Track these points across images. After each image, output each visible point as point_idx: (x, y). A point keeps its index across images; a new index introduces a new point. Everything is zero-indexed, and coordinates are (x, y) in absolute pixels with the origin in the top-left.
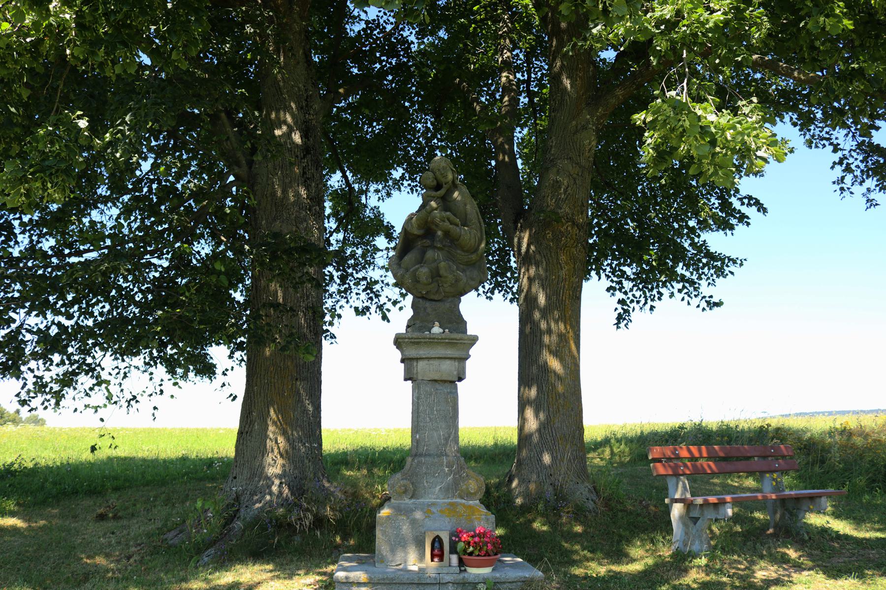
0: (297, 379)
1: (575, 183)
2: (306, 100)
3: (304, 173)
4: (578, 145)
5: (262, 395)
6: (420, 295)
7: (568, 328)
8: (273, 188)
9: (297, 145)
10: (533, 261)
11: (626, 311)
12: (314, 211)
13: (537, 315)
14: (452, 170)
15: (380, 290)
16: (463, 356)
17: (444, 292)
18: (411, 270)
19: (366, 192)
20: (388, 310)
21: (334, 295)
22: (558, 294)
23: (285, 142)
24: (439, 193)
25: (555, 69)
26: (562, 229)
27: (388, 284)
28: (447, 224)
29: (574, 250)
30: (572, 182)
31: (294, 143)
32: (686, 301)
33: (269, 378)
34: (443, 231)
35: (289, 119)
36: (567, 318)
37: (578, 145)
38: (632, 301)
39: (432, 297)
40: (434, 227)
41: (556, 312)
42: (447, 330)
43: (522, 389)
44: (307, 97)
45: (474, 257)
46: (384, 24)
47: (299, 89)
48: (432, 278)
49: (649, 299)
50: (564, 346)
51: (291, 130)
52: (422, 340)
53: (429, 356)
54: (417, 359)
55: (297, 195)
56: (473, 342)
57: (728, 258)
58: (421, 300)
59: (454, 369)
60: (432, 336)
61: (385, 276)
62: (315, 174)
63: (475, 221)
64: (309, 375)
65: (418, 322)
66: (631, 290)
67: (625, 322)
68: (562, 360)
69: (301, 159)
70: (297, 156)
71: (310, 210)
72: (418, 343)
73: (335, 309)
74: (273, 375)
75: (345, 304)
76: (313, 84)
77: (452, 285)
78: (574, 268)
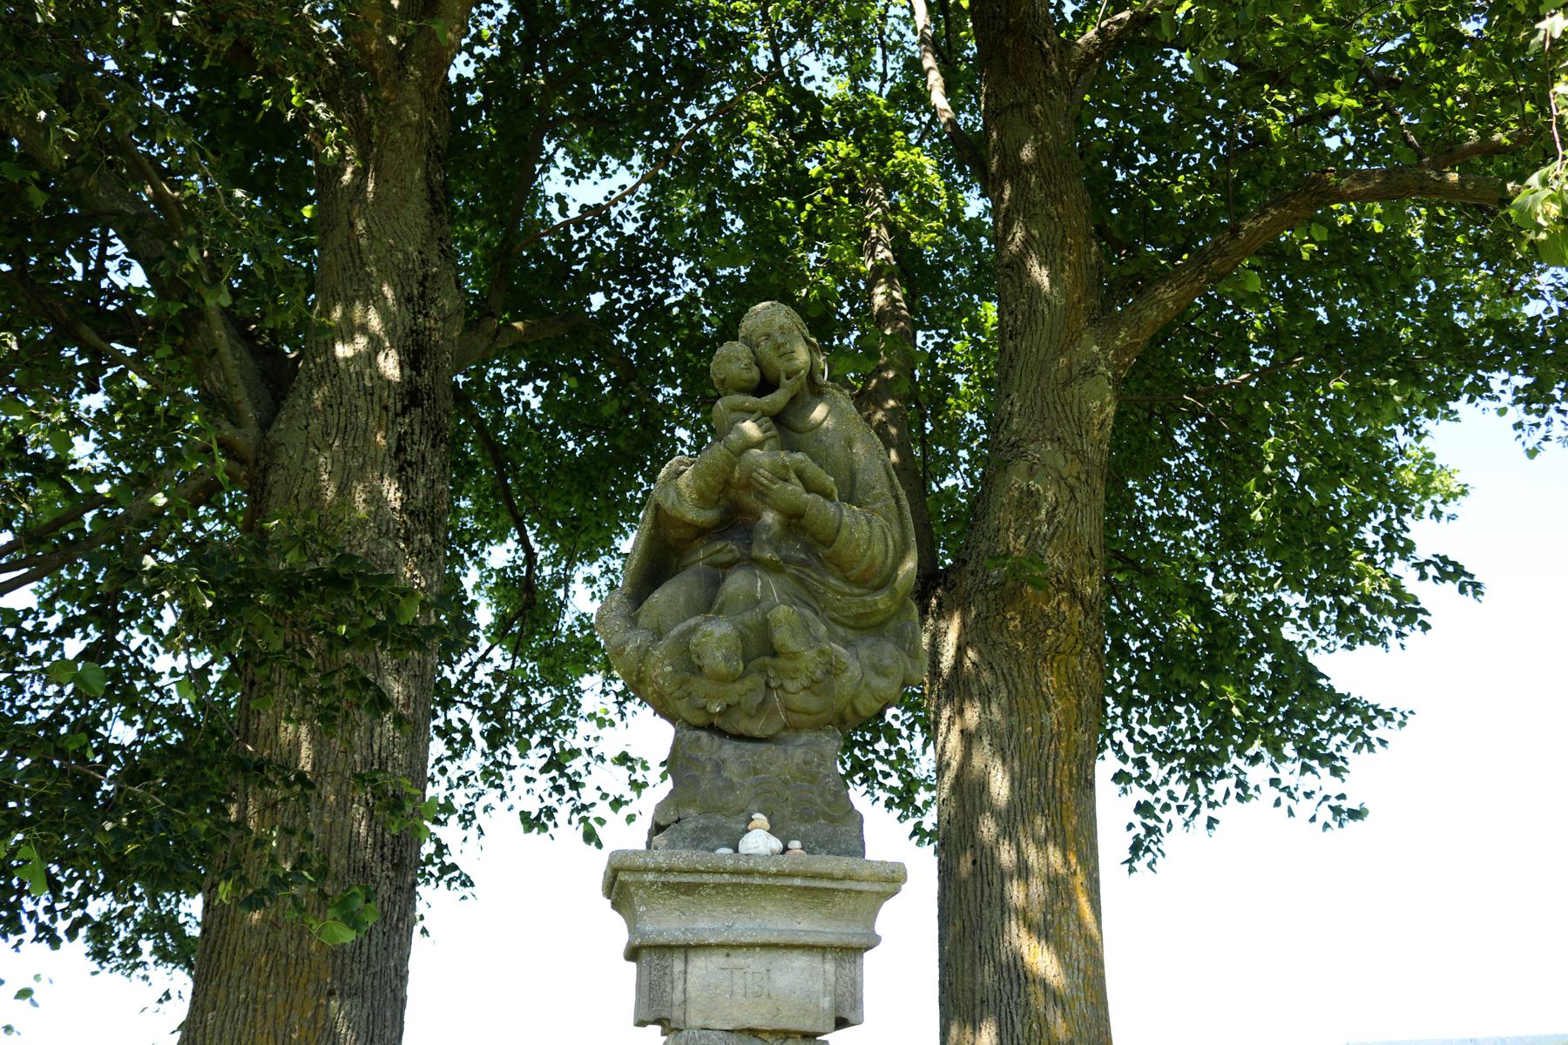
0: (331, 993)
1: (1073, 498)
2: (421, 284)
3: (400, 449)
4: (1075, 410)
5: (227, 1036)
6: (699, 719)
7: (1073, 860)
8: (317, 481)
9: (389, 382)
10: (975, 689)
11: (1150, 831)
12: (417, 545)
13: (988, 828)
14: (808, 342)
15: (584, 772)
16: (855, 941)
17: (787, 709)
18: (674, 632)
19: (566, 581)
20: (601, 821)
21: (472, 779)
22: (1042, 773)
23: (360, 375)
24: (768, 399)
25: (1013, 248)
26: (1047, 609)
27: (601, 758)
28: (795, 488)
29: (1075, 661)
30: (1066, 495)
31: (381, 377)
32: (1283, 809)
33: (252, 988)
34: (780, 512)
35: (375, 322)
36: (1069, 835)
37: (1075, 410)
38: (1166, 807)
39: (745, 726)
40: (750, 500)
41: (1039, 821)
42: (795, 845)
43: (954, 1031)
44: (425, 277)
45: (882, 600)
46: (620, 220)
48: (747, 660)
49: (1204, 803)
50: (1064, 911)
51: (376, 345)
52: (707, 878)
53: (730, 937)
54: (687, 949)
55: (376, 499)
56: (888, 887)
57: (1375, 707)
58: (703, 735)
59: (819, 987)
60: (743, 865)
61: (597, 739)
62: (428, 456)
63: (881, 488)
64: (368, 980)
65: (692, 812)
66: (1165, 782)
67: (1149, 856)
68: (1060, 949)
69: (397, 415)
70: (386, 408)
71: (406, 540)
72: (690, 889)
73: (472, 813)
74: (262, 980)
75: (496, 802)
76: (443, 251)
77: (812, 687)
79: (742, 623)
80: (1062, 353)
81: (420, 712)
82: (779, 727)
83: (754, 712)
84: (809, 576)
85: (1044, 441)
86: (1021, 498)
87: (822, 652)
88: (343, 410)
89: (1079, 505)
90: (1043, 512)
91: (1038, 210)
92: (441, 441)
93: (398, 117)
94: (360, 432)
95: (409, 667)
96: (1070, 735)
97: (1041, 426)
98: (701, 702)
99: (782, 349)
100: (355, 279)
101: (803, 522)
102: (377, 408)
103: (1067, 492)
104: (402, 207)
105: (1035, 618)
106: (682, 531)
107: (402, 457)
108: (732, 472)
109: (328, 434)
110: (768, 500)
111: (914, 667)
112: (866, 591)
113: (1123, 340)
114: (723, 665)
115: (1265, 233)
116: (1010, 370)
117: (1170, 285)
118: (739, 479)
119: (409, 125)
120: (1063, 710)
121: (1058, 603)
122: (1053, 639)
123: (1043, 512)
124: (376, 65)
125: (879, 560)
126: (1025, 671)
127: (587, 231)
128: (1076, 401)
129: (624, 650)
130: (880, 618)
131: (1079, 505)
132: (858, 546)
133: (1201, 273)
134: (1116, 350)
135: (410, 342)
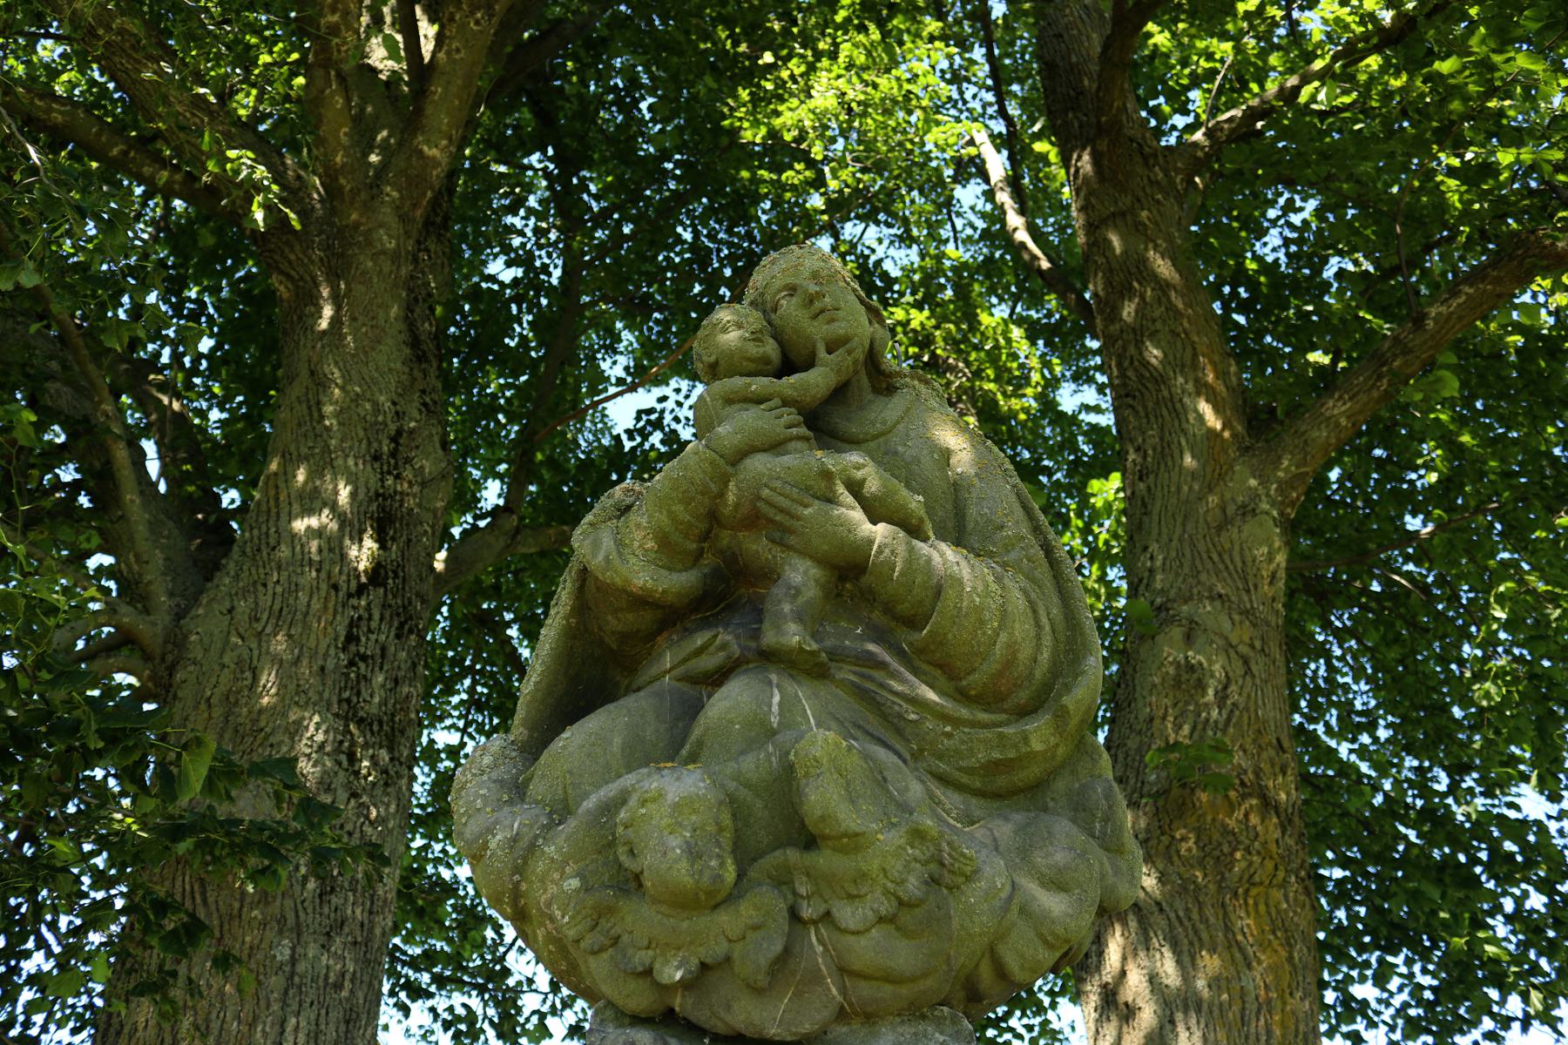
1: (1248, 671)
3: (351, 638)
6: (639, 999)
17: (844, 971)
26: (1231, 823)
29: (1277, 894)
30: (1239, 668)
34: (821, 561)
40: (758, 547)
44: (399, 432)
45: (1039, 734)
47: (377, 409)
48: (745, 856)
69: (350, 595)
70: (336, 587)
76: (425, 405)
78: (1290, 959)
79: (737, 777)
80: (1211, 490)
81: (360, 995)
82: (826, 1014)
83: (762, 980)
84: (882, 686)
85: (1200, 600)
86: (1179, 675)
87: (918, 835)
88: (279, 589)
89: (1258, 681)
90: (1211, 692)
91: (1158, 325)
92: (411, 631)
93: (369, 243)
94: (299, 616)
95: (346, 930)
96: (1284, 1003)
97: (1194, 582)
98: (641, 958)
99: (818, 305)
100: (311, 434)
101: (866, 580)
102: (324, 586)
103: (1240, 663)
104: (373, 349)
105: (1216, 836)
106: (630, 617)
107: (353, 648)
108: (722, 495)
109: (258, 620)
110: (792, 540)
111: (1117, 871)
112: (1004, 717)
113: (1286, 470)
114: (684, 865)
115: (1460, 318)
116: (1146, 519)
117: (1340, 397)
118: (737, 506)
119: (384, 252)
120: (1270, 966)
121: (1244, 815)
122: (1244, 864)
123: (1211, 692)
124: (343, 181)
125: (1025, 654)
126: (1209, 912)
127: (639, 439)
128: (1237, 548)
129: (485, 846)
130: (1034, 772)
131: (1258, 681)
132: (982, 622)
133: (1380, 377)
134: (1280, 482)
135: (374, 507)
